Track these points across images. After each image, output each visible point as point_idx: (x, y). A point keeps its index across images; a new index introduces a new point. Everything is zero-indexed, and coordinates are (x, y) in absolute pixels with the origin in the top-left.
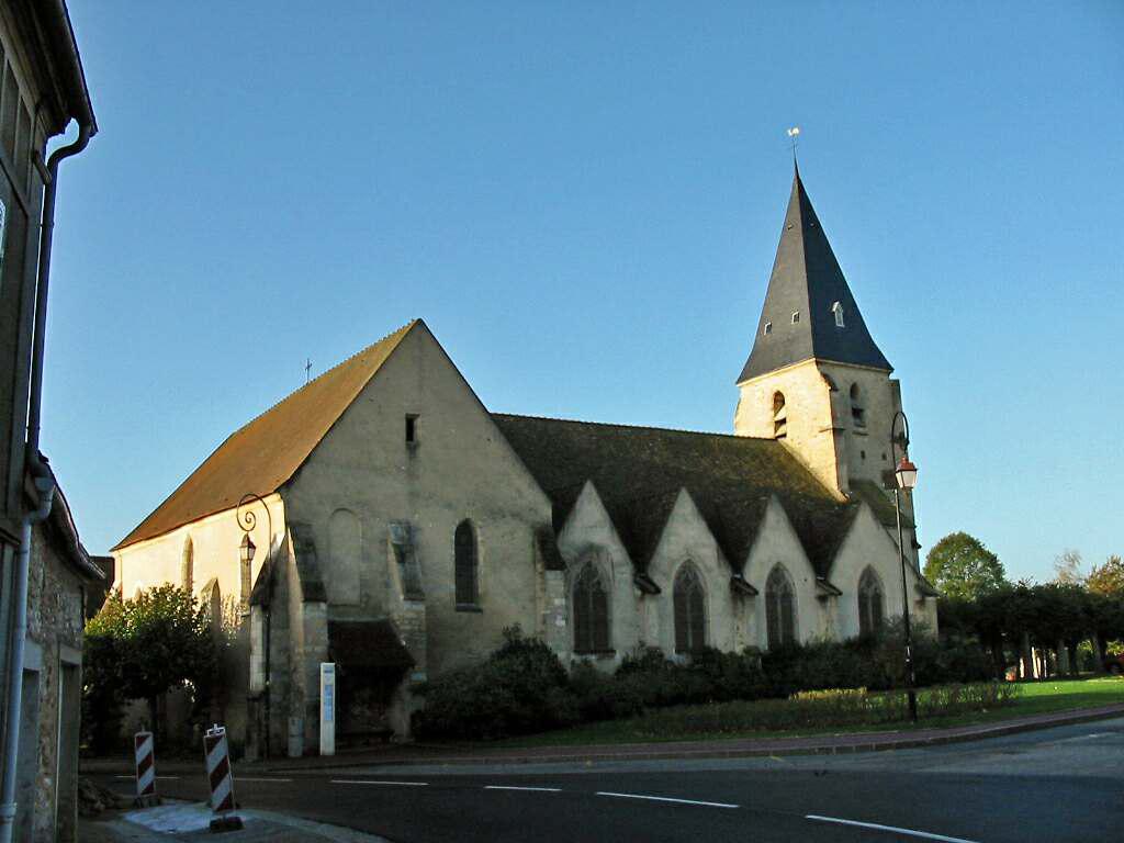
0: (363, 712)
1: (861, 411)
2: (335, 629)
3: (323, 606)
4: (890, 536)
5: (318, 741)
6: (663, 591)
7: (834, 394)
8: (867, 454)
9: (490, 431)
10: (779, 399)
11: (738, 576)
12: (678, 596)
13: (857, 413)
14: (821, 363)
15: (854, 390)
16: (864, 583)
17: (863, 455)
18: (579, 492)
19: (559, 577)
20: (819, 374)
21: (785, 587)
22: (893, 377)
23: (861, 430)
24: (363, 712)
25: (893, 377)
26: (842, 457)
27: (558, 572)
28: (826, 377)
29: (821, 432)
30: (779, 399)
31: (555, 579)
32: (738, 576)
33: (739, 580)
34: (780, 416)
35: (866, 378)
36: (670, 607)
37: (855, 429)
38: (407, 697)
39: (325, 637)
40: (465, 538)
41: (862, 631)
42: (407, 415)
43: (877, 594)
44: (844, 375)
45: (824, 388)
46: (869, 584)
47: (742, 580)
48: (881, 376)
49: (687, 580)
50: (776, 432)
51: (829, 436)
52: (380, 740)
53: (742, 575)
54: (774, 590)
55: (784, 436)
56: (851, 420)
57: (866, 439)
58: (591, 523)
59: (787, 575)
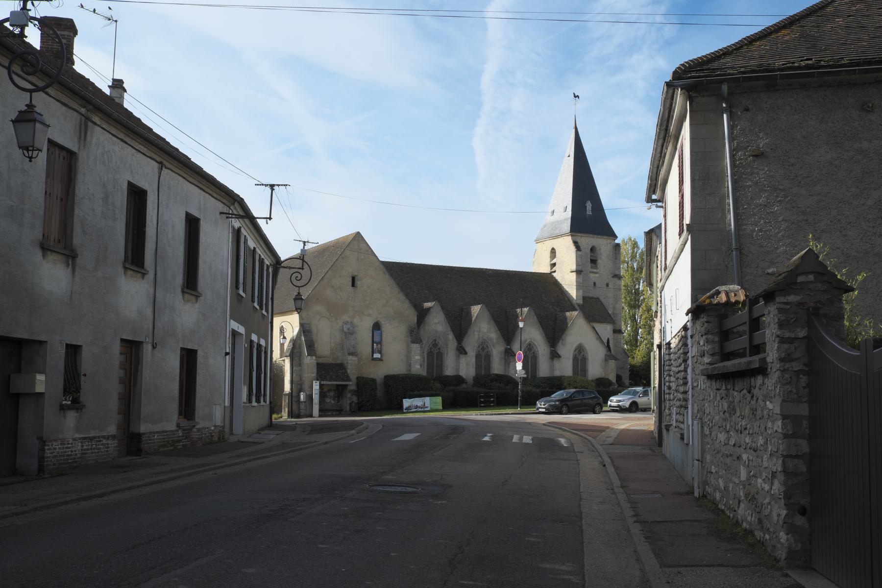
0: (331, 401)
2: (319, 365)
3: (314, 358)
4: (594, 328)
5: (312, 412)
6: (468, 353)
7: (579, 253)
8: (597, 284)
9: (249, 341)
10: (553, 252)
11: (509, 347)
12: (478, 356)
13: (594, 261)
14: (575, 235)
15: (593, 249)
16: (577, 351)
17: (595, 284)
18: (555, 278)
19: (418, 346)
20: (572, 242)
21: (534, 353)
22: (617, 241)
23: (595, 270)
24: (331, 401)
25: (617, 241)
26: (579, 287)
27: (418, 344)
28: (576, 243)
29: (571, 272)
30: (553, 252)
31: (416, 347)
32: (509, 347)
33: (509, 349)
34: (553, 262)
35: (602, 243)
36: (474, 360)
37: (592, 270)
38: (349, 395)
39: (315, 370)
40: (377, 326)
41: (477, 373)
43: (584, 358)
44: (587, 241)
45: (573, 249)
46: (580, 352)
47: (510, 349)
48: (609, 241)
49: (483, 349)
50: (551, 269)
51: (574, 274)
52: (337, 413)
53: (510, 347)
54: (528, 354)
55: (555, 272)
56: (589, 265)
57: (597, 275)
58: (437, 323)
59: (535, 347)
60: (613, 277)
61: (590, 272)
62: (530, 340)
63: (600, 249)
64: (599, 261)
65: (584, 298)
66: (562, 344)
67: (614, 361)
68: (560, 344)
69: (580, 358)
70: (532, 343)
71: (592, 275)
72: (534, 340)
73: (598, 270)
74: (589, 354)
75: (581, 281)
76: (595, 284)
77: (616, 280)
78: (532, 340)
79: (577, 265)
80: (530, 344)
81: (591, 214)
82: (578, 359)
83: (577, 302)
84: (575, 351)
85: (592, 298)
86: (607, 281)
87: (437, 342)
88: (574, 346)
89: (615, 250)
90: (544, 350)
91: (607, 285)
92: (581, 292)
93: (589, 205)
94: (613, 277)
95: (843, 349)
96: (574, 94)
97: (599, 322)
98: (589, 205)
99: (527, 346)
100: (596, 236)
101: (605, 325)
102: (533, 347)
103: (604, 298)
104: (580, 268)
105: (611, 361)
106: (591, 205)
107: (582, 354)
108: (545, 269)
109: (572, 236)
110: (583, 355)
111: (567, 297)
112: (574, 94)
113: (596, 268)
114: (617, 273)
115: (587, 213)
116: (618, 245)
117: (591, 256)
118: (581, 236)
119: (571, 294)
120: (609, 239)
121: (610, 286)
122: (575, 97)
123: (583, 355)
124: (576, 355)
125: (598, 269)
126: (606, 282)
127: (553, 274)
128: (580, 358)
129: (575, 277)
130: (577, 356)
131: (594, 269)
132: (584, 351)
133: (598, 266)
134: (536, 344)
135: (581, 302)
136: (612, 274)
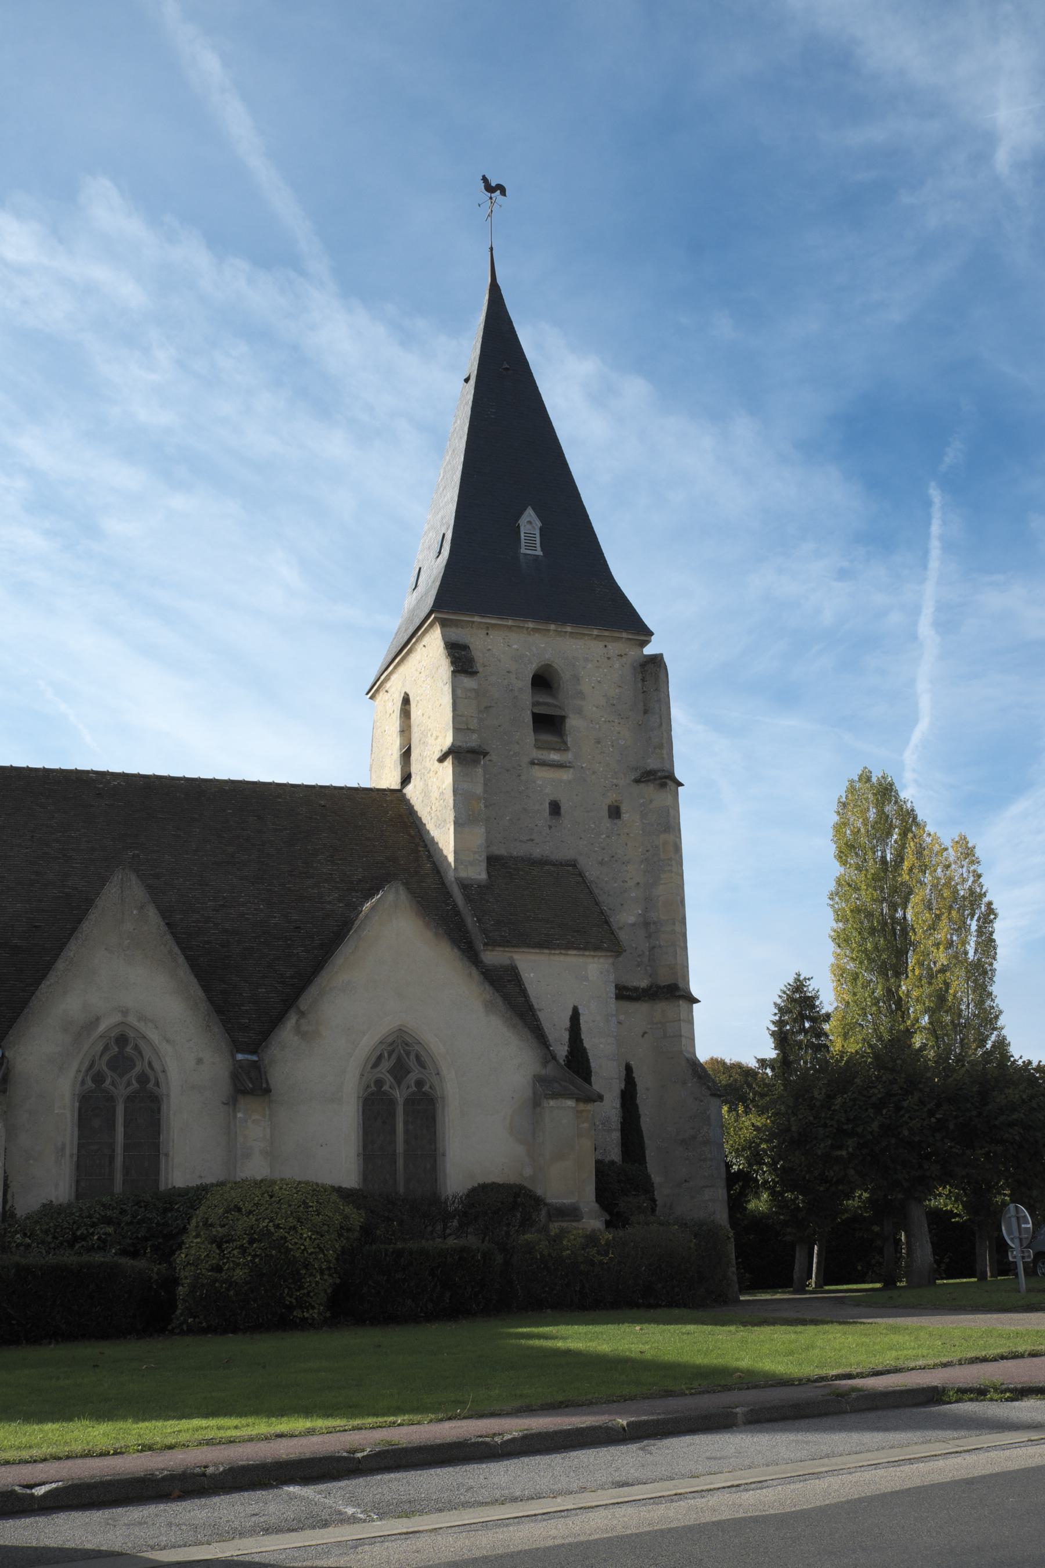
1: (562, 719)
7: (467, 682)
16: (386, 1065)
17: (555, 808)
21: (143, 1079)
23: (554, 756)
25: (649, 650)
42: (661, 655)
46: (400, 1071)
48: (614, 648)
56: (527, 734)
57: (565, 775)
59: (147, 1053)
60: (637, 781)
61: (532, 763)
62: (117, 1018)
63: (576, 679)
64: (573, 723)
65: (493, 861)
66: (298, 1030)
67: (570, 1103)
68: (287, 1033)
69: (400, 1096)
70: (131, 1034)
71: (541, 774)
72: (142, 1018)
73: (569, 756)
74: (449, 1075)
75: (479, 790)
76: (555, 808)
77: (649, 790)
78: (132, 1019)
79: (457, 730)
80: (122, 1040)
81: (539, 552)
82: (392, 1102)
83: (463, 874)
84: (375, 1065)
85: (542, 863)
86: (611, 797)
87: (129, 1049)
88: (368, 1042)
89: (643, 680)
90: (200, 1061)
91: (615, 812)
92: (478, 836)
93: (530, 524)
94: (637, 781)
95: (988, 1269)
96: (485, 179)
97: (544, 944)
98: (530, 524)
99: (106, 1048)
100: (552, 627)
101: (571, 960)
102: (136, 1047)
103: (601, 863)
104: (473, 741)
105: (552, 1103)
106: (539, 524)
107: (412, 1078)
108: (390, 780)
109: (444, 624)
110: (420, 1083)
111: (434, 863)
112: (485, 179)
113: (563, 748)
114: (652, 764)
115: (523, 551)
116: (657, 661)
117: (535, 704)
118: (488, 626)
119: (440, 845)
120: (620, 638)
121: (625, 816)
122: (490, 188)
123: (420, 1083)
124: (379, 1083)
125: (567, 749)
126: (608, 801)
127: (1041, 1064)
128: (400, 1096)
129: (449, 780)
130: (386, 1088)
131: (559, 750)
132: (422, 1064)
133: (569, 740)
134: (154, 1036)
135: (478, 873)
136: (636, 769)
